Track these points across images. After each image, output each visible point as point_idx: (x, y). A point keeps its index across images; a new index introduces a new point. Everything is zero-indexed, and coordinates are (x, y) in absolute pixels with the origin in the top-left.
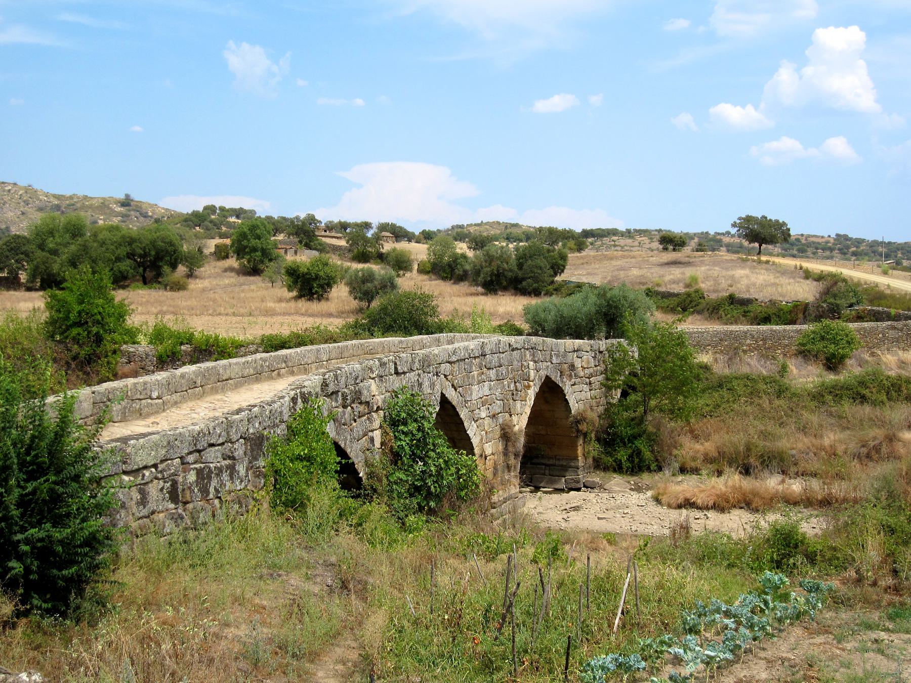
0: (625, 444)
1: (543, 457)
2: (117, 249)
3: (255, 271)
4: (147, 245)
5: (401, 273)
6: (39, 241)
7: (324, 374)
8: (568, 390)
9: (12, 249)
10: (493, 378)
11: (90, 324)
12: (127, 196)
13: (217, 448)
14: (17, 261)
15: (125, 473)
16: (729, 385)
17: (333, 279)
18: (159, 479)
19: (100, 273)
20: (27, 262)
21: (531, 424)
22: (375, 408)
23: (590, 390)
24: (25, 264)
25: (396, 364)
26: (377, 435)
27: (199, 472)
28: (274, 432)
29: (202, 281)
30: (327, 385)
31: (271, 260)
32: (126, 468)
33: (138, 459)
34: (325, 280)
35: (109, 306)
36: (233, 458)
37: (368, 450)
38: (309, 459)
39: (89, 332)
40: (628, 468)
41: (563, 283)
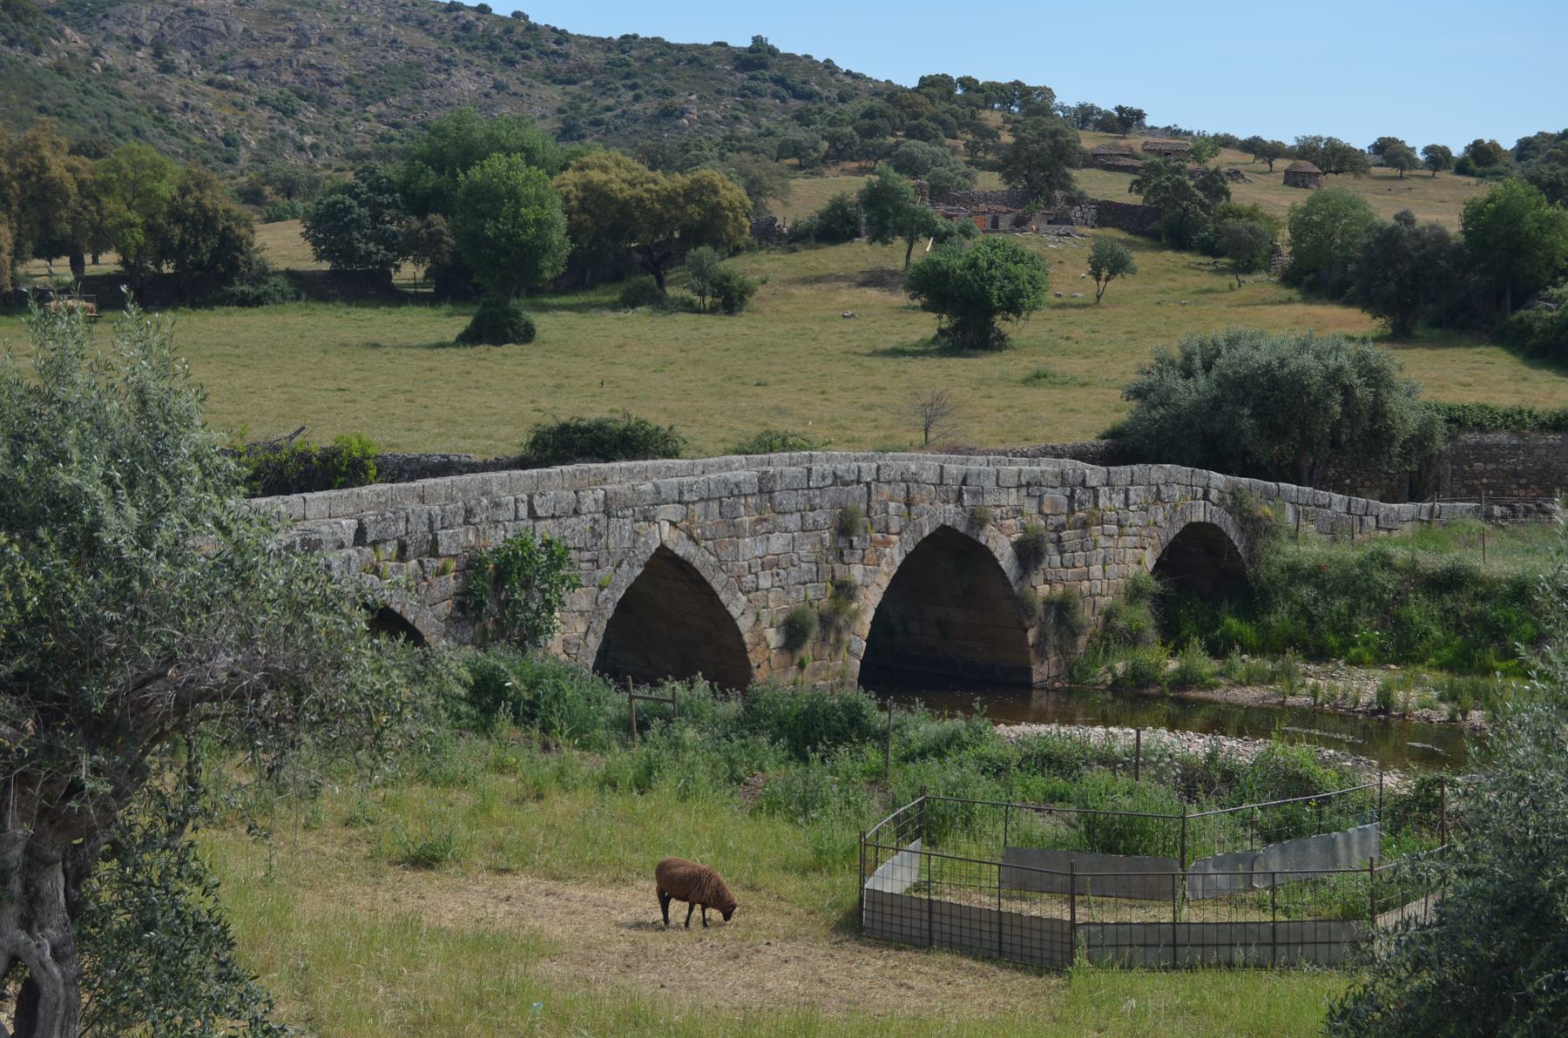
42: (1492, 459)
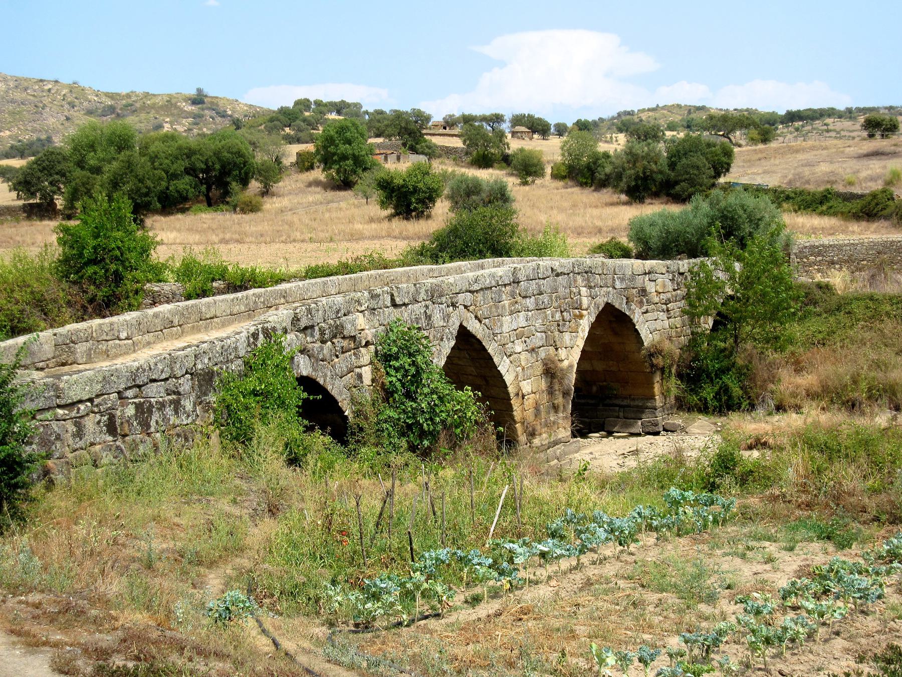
0: (712, 381)
1: (616, 397)
2: (173, 163)
3: (346, 185)
4: (211, 157)
5: (530, 179)
6: (77, 157)
7: (296, 308)
8: (637, 317)
9: (44, 168)
10: (531, 308)
11: (108, 261)
12: (199, 91)
13: (159, 383)
14: (51, 183)
15: (59, 406)
16: (849, 308)
17: (435, 191)
18: (96, 413)
19: (118, 202)
20: (64, 183)
21: (459, 349)
22: (363, 343)
23: (668, 318)
24: (62, 186)
25: (392, 295)
26: (367, 373)
27: (138, 407)
28: (227, 368)
29: (279, 199)
30: (298, 320)
31: (365, 169)
32: (60, 402)
33: (72, 393)
34: (426, 193)
35: (130, 239)
36: (179, 393)
37: (355, 387)
38: (266, 394)
39: (107, 271)
40: (715, 408)
41: (727, 186)
42: (819, 254)
